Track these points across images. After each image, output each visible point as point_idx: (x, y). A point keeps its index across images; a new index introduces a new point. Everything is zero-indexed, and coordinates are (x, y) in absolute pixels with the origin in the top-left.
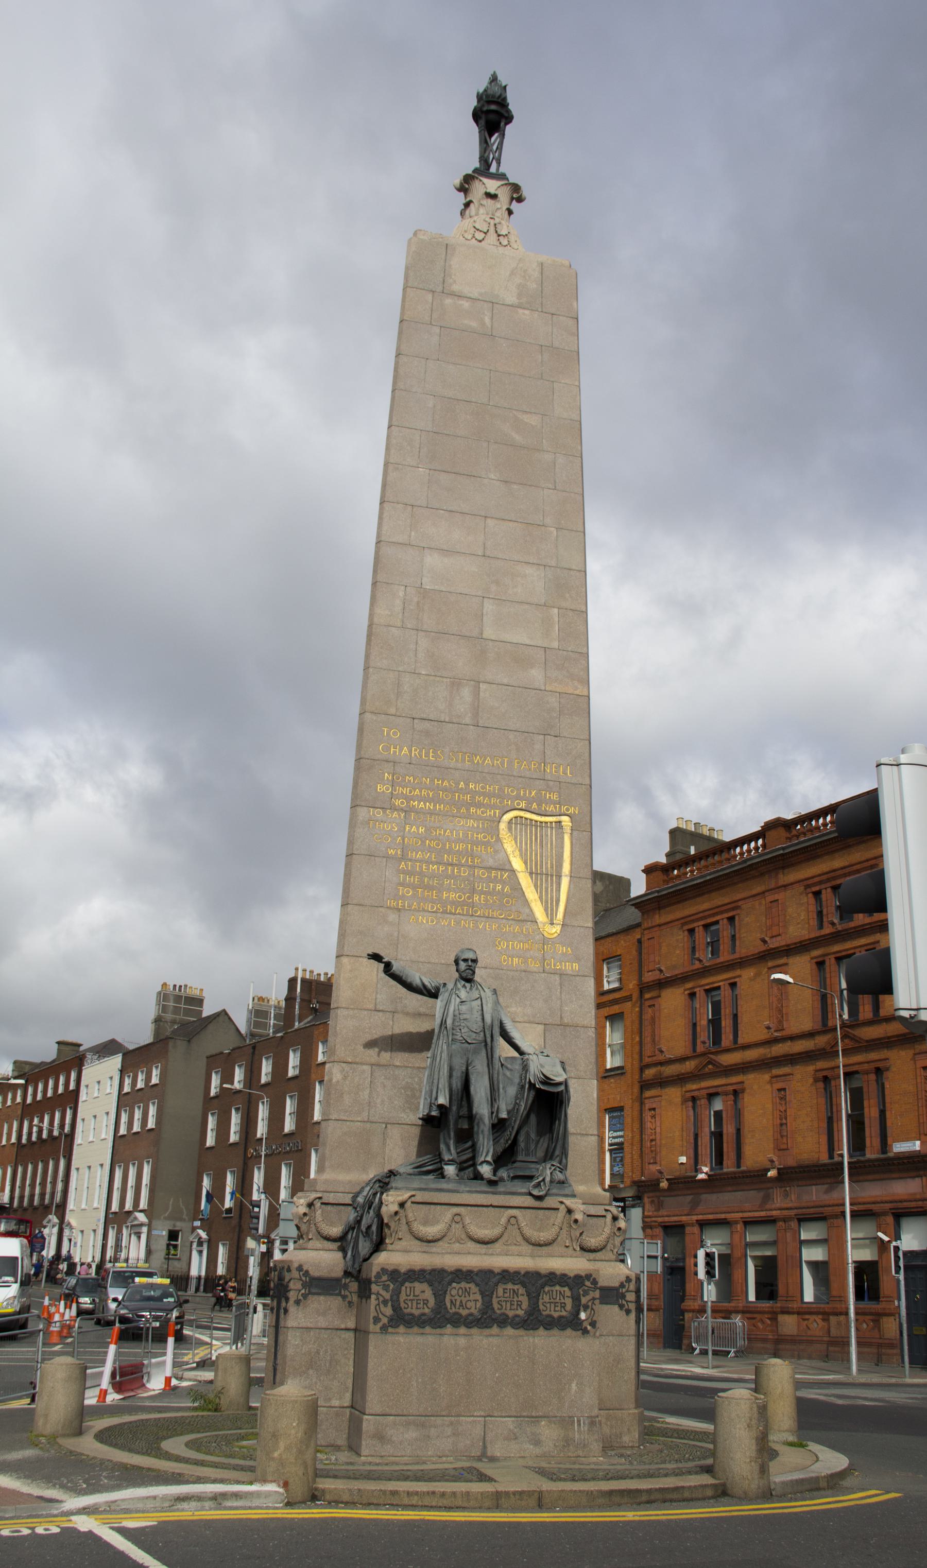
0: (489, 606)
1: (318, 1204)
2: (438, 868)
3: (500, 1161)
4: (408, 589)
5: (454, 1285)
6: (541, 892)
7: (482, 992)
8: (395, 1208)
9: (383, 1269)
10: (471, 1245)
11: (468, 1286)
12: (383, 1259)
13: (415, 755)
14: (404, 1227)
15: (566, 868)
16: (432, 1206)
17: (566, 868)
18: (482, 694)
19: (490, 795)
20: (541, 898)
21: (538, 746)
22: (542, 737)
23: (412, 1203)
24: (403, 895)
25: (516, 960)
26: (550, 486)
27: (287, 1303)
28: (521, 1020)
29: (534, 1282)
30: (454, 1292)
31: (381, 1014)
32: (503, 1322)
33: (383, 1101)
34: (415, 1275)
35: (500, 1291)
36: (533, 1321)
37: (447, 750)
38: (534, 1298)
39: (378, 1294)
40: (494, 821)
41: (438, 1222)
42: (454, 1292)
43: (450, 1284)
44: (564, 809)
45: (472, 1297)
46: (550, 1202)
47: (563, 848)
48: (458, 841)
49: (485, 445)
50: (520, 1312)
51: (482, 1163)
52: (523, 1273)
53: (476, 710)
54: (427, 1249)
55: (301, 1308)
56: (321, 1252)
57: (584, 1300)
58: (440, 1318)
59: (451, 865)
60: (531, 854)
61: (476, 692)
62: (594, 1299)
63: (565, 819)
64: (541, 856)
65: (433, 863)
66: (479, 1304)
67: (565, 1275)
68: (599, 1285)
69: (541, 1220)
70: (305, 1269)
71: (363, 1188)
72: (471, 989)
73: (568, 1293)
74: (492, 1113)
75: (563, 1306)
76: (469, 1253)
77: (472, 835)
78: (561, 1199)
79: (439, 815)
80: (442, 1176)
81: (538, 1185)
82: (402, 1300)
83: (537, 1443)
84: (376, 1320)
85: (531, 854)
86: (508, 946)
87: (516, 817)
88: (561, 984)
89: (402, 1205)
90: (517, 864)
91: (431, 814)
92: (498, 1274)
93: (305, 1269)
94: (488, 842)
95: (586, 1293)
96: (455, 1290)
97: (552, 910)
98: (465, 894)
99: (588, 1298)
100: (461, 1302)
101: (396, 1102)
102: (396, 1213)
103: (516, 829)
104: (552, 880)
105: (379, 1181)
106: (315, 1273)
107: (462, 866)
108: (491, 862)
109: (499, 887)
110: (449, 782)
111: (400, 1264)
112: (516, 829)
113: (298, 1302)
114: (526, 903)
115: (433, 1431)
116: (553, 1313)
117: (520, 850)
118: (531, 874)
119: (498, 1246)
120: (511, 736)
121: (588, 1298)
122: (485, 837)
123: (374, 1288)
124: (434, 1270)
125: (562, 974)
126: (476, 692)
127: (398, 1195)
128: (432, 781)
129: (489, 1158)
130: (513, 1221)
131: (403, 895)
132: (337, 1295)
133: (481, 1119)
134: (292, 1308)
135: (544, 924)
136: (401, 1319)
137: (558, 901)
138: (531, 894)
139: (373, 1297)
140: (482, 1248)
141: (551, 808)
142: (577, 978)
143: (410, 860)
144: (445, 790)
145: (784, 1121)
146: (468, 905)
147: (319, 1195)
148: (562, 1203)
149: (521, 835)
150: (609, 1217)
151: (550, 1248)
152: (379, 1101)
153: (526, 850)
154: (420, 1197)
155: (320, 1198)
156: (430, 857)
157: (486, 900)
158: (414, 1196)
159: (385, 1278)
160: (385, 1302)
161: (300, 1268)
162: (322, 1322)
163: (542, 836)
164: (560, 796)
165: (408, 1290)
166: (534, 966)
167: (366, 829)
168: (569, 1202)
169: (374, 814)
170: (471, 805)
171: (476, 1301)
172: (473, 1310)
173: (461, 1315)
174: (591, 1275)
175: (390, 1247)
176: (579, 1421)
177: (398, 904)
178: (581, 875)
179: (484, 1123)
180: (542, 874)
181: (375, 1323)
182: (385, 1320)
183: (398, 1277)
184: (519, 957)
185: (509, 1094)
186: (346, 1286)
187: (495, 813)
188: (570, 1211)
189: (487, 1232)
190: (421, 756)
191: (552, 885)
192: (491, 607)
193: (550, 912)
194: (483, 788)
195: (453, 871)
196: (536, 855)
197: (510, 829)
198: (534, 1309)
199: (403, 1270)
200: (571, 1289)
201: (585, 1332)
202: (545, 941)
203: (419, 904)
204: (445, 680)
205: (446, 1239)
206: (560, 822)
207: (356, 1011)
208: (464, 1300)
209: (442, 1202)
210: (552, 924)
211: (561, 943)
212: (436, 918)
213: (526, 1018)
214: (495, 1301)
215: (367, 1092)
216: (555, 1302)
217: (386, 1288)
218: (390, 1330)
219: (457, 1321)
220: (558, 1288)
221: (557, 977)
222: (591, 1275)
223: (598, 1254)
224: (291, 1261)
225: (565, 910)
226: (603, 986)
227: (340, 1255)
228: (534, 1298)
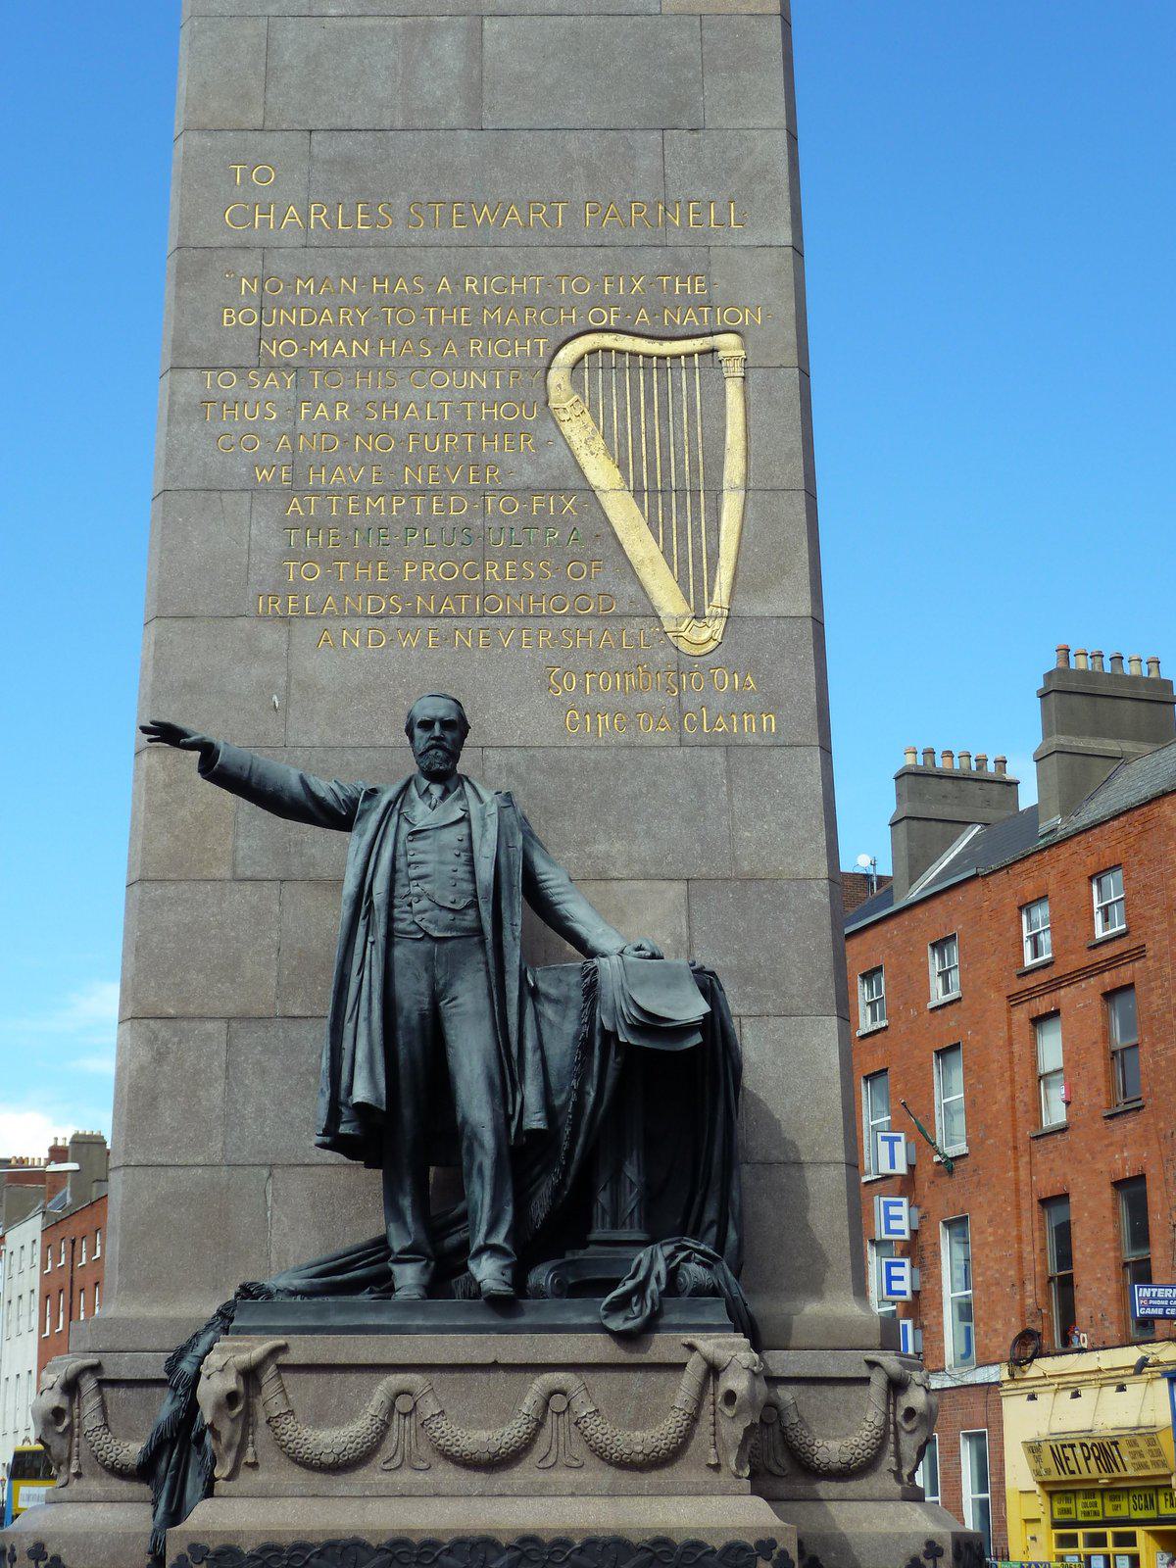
1: (89, 1384)
2: (389, 505)
3: (524, 1255)
6: (667, 539)
8: (231, 1383)
9: (193, 1547)
10: (449, 1476)
13: (318, 223)
15: (734, 468)
16: (337, 1377)
17: (734, 468)
20: (667, 553)
21: (646, 163)
22: (656, 136)
24: (299, 581)
28: (625, 873)
31: (248, 887)
33: (260, 1111)
37: (401, 200)
41: (352, 1415)
44: (722, 318)
46: (663, 1346)
47: (722, 417)
48: (441, 429)
51: (481, 1251)
52: (578, 1543)
53: (475, 92)
56: (99, 1507)
59: (423, 492)
60: (637, 441)
61: (474, 45)
63: (728, 343)
64: (665, 446)
67: (697, 1545)
69: (640, 1398)
71: (196, 1336)
72: (443, 798)
76: (437, 1495)
77: (477, 411)
78: (688, 1338)
79: (386, 369)
85: (637, 441)
86: (581, 686)
87: (592, 352)
88: (728, 772)
89: (251, 1375)
90: (600, 471)
91: (366, 368)
92: (510, 1547)
94: (521, 421)
97: (699, 581)
98: (461, 563)
101: (295, 1110)
103: (593, 381)
104: (696, 504)
107: (453, 491)
108: (528, 475)
110: (409, 282)
111: (239, 1533)
112: (593, 381)
114: (628, 569)
117: (606, 436)
118: (637, 493)
119: (518, 1476)
120: (573, 142)
122: (510, 413)
125: (730, 746)
126: (474, 45)
127: (239, 1350)
128: (365, 283)
129: (499, 1239)
130: (558, 1404)
131: (299, 581)
133: (475, 1137)
135: (678, 620)
138: (640, 545)
140: (478, 1480)
141: (689, 319)
142: (776, 753)
143: (315, 491)
144: (400, 303)
147: (92, 1360)
148: (692, 1348)
149: (607, 396)
150: (878, 1380)
151: (666, 1473)
152: (250, 1109)
153: (623, 432)
154: (302, 1349)
155: (95, 1369)
156: (367, 478)
157: (520, 574)
158: (283, 1349)
163: (663, 393)
164: (710, 285)
166: (653, 732)
167: (196, 426)
169: (214, 385)
170: (469, 333)
178: (776, 483)
179: (482, 1146)
180: (653, 492)
184: (613, 713)
187: (536, 348)
188: (713, 1370)
189: (483, 1435)
190: (333, 224)
191: (696, 518)
193: (694, 582)
195: (428, 506)
196: (650, 443)
197: (576, 383)
202: (682, 664)
203: (340, 600)
204: (391, 22)
205: (379, 1460)
206: (713, 351)
207: (184, 886)
209: (362, 1360)
210: (699, 616)
211: (726, 665)
212: (385, 630)
215: (218, 1090)
221: (718, 755)
222: (772, 1543)
223: (853, 1484)
225: (735, 577)
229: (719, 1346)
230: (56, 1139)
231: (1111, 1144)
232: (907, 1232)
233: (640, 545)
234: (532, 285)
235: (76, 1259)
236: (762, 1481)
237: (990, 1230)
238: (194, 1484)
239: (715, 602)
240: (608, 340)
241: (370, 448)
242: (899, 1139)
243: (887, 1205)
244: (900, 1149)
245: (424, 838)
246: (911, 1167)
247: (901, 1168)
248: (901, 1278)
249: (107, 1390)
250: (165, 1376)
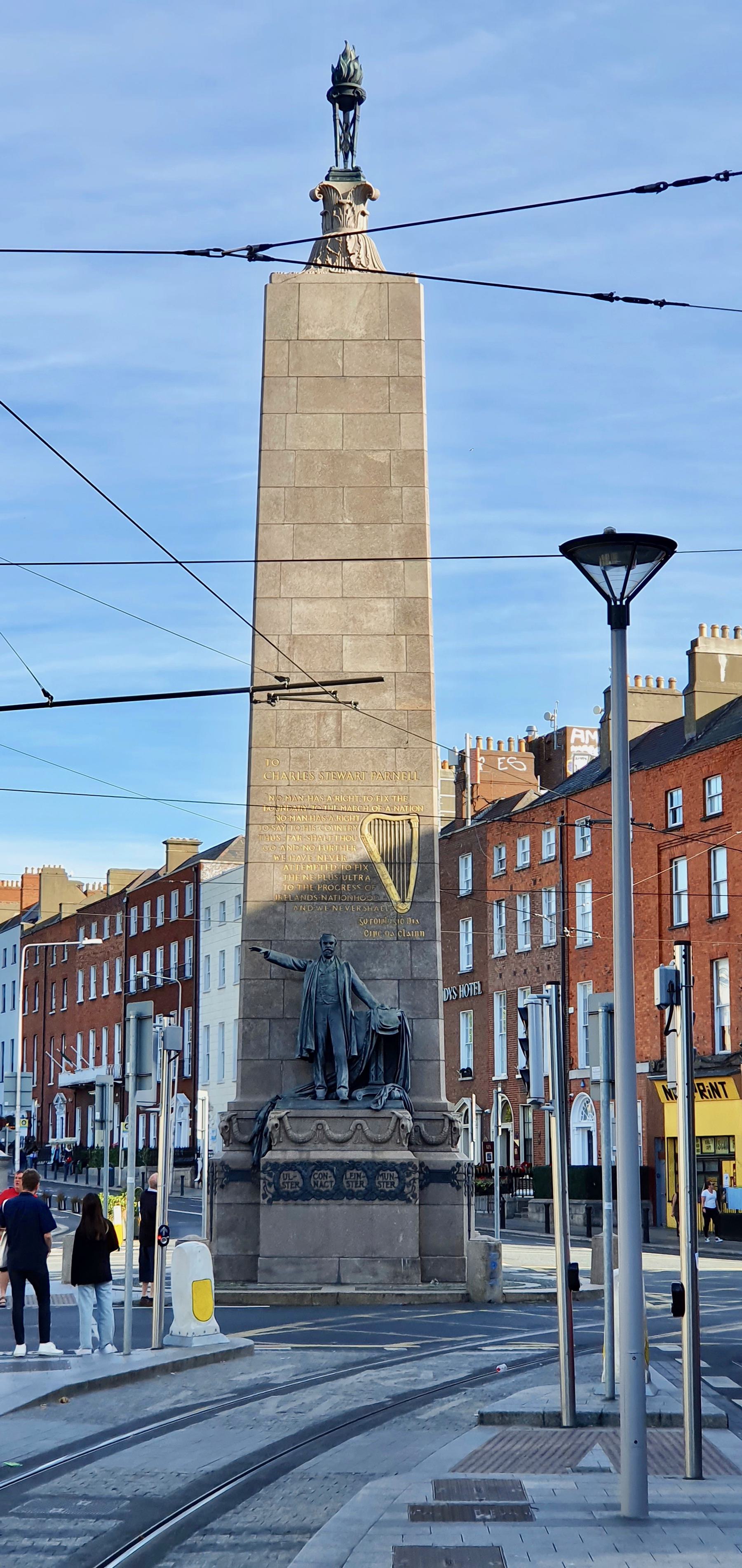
0: (347, 642)
1: (234, 1120)
3: (354, 1085)
4: (281, 637)
11: (325, 1172)
18: (343, 720)
20: (394, 882)
21: (390, 759)
25: (375, 933)
26: (398, 521)
29: (375, 1168)
30: (316, 1176)
31: (274, 981)
32: (351, 1195)
34: (290, 1166)
35: (348, 1174)
36: (371, 1194)
38: (371, 1179)
39: (265, 1179)
43: (313, 1171)
45: (329, 1179)
49: (340, 491)
50: (362, 1188)
54: (300, 1148)
58: (305, 1194)
62: (414, 1179)
65: (308, 864)
67: (393, 1163)
73: (396, 1175)
75: (393, 1184)
80: (315, 1097)
83: (375, 1274)
84: (265, 1196)
95: (408, 1176)
96: (317, 1174)
97: (403, 891)
99: (411, 1178)
106: (233, 1167)
109: (361, 877)
114: (383, 888)
115: (304, 1268)
118: (386, 864)
121: (411, 1178)
125: (412, 941)
130: (359, 1127)
136: (279, 1195)
138: (388, 880)
139: (262, 1181)
146: (338, 893)
154: (293, 1113)
157: (351, 888)
160: (270, 1184)
162: (239, 1200)
166: (389, 936)
171: (332, 1182)
172: (330, 1188)
176: (404, 1261)
180: (395, 863)
181: (264, 1198)
182: (270, 1196)
183: (276, 1166)
184: (378, 930)
185: (358, 1039)
188: (399, 1119)
192: (349, 643)
193: (402, 893)
199: (281, 1163)
200: (398, 1173)
202: (398, 916)
205: (313, 1141)
208: (323, 1181)
210: (404, 902)
213: (384, 976)
216: (350, 1179)
217: (270, 1175)
219: (320, 1196)
220: (388, 1172)
221: (408, 943)
227: (250, 1153)
230: (26, 869)
231: (710, 938)
233: (388, 880)
235: (49, 961)
236: (411, 1146)
237: (644, 983)
238: (265, 1147)
240: (378, 816)
249: (240, 1121)
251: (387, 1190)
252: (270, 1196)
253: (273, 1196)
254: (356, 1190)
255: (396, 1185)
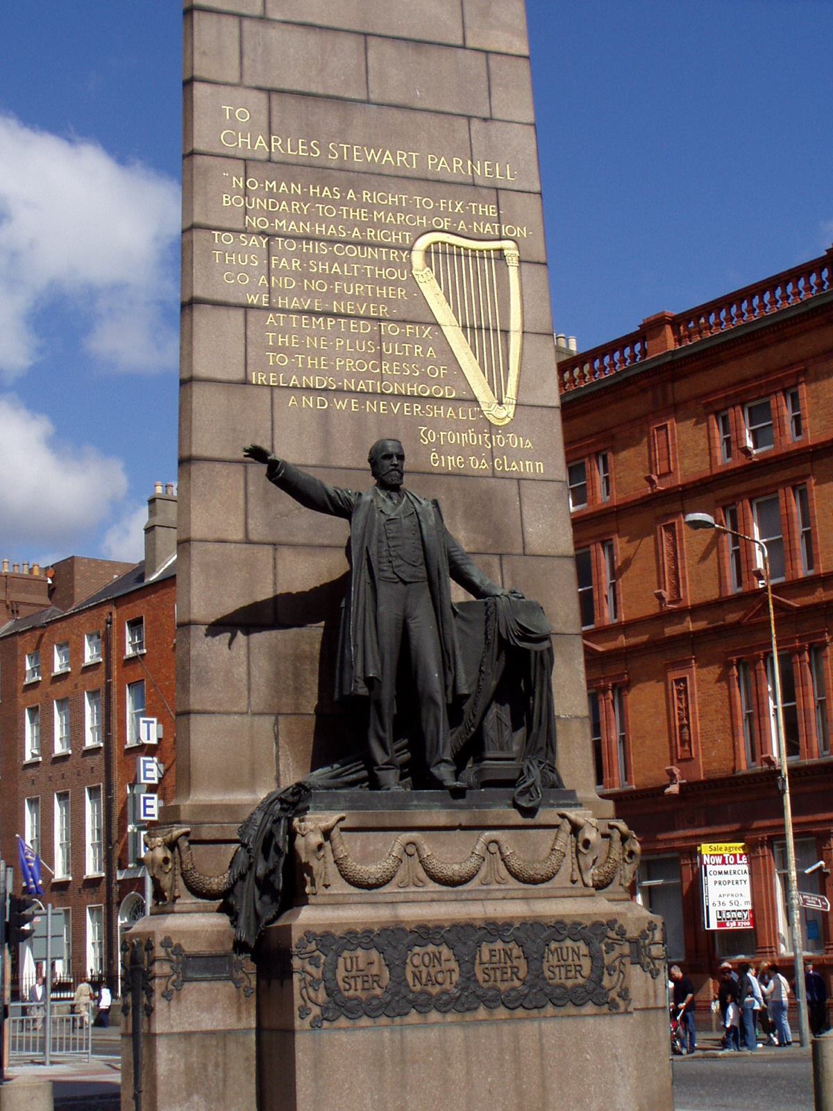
5: (417, 949)
7: (416, 505)
8: (317, 839)
10: (433, 886)
12: (307, 917)
14: (333, 869)
19: (396, 210)
23: (342, 830)
27: (149, 997)
29: (537, 936)
38: (534, 959)
40: (403, 250)
42: (417, 961)
43: (409, 948)
46: (544, 816)
55: (173, 1003)
57: (608, 959)
58: (398, 1002)
63: (508, 245)
66: (455, 977)
68: (628, 935)
70: (175, 942)
73: (584, 950)
74: (446, 687)
77: (373, 271)
81: (526, 791)
82: (339, 979)
87: (436, 243)
89: (327, 834)
90: (442, 312)
92: (411, 932)
93: (175, 942)
95: (610, 948)
96: (418, 955)
99: (614, 954)
100: (429, 974)
102: (320, 847)
105: (282, 801)
106: (189, 947)
113: (167, 995)
116: (499, 984)
122: (392, 274)
123: (296, 963)
124: (384, 930)
127: (320, 820)
132: (227, 979)
134: (160, 1005)
136: (341, 1007)
137: (507, 368)
139: (296, 977)
143: (283, 311)
145: (685, 722)
148: (563, 816)
149: (445, 271)
155: (187, 834)
158: (342, 819)
159: (313, 946)
160: (314, 984)
161: (166, 943)
165: (349, 961)
168: (572, 814)
171: (451, 971)
172: (447, 986)
173: (430, 995)
174: (615, 921)
175: (312, 899)
177: (268, 379)
183: (326, 940)
186: (239, 966)
188: (576, 829)
193: (497, 386)
194: (382, 198)
198: (536, 978)
199: (338, 933)
200: (588, 944)
201: (613, 1005)
214: (478, 970)
217: (314, 962)
218: (326, 1024)
222: (615, 921)
224: (152, 934)
226: (124, 651)
228: (534, 959)
229: (577, 815)
232: (156, 779)
234: (400, 200)
239: (508, 395)
241: (313, 288)
242: (153, 722)
243: (145, 762)
244: (153, 727)
245: (394, 523)
246: (159, 740)
247: (154, 741)
248: (152, 807)
250: (238, 837)
251: (570, 983)
252: (316, 1011)
253: (325, 1009)
254: (503, 987)
255: (522, 974)
